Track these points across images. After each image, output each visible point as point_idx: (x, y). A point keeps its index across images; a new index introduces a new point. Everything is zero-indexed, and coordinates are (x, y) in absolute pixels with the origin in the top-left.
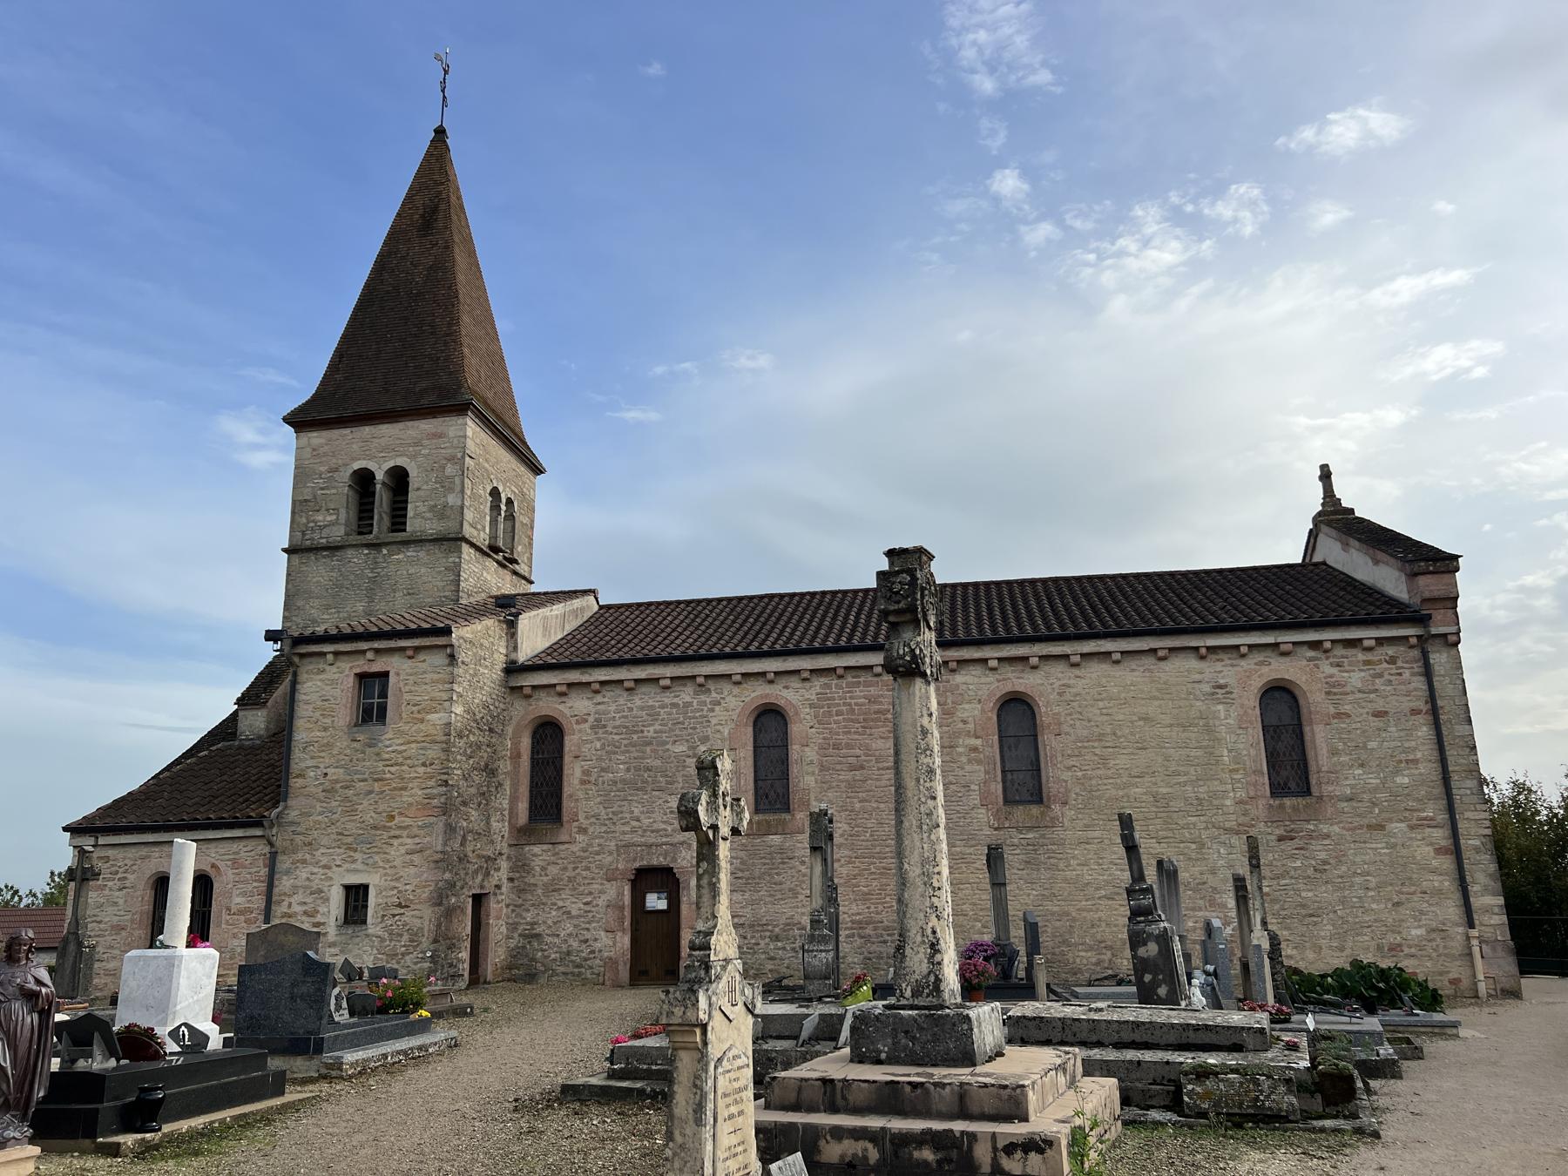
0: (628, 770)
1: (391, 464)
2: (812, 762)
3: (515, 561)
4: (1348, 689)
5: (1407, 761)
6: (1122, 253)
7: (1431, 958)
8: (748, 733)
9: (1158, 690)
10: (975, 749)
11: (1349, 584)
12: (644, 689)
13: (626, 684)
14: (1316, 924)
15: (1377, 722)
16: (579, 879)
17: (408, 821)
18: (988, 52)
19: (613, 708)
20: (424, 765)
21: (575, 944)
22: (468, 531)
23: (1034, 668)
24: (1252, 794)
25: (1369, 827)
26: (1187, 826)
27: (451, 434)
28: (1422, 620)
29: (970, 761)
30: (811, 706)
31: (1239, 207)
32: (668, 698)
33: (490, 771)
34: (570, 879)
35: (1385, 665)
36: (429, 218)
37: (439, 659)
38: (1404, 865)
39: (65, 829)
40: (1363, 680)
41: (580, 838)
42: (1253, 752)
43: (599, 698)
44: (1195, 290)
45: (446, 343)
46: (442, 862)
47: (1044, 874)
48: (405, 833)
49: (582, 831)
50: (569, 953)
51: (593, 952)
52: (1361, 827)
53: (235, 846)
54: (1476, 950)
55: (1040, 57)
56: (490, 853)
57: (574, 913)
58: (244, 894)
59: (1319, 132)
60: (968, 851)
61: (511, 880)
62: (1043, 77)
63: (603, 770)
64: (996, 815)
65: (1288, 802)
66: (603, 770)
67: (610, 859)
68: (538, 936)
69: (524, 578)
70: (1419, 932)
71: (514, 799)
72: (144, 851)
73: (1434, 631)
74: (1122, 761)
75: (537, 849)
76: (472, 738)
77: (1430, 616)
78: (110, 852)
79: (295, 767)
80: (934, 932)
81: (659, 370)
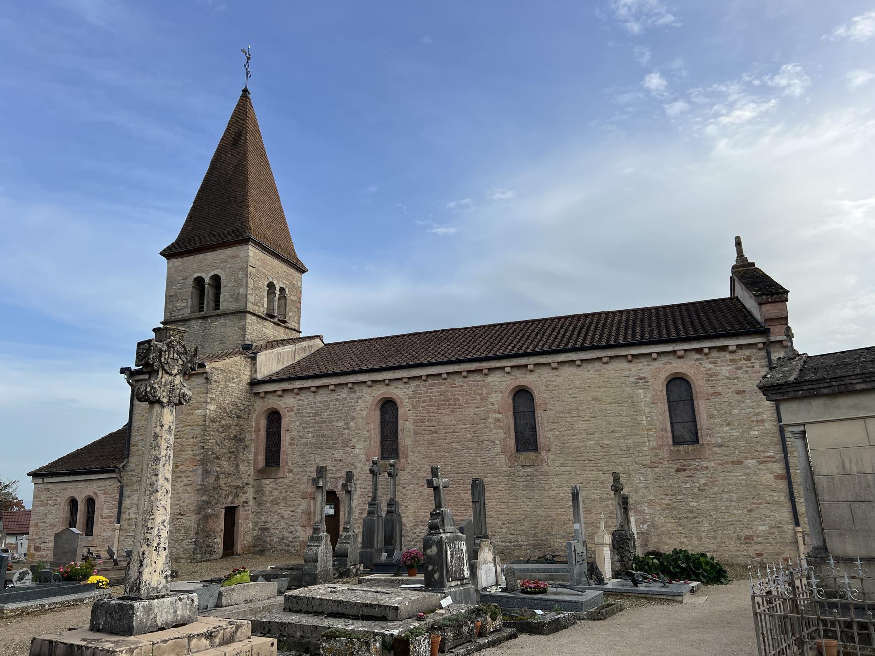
0: (313, 437)
1: (212, 273)
2: (409, 430)
3: (284, 322)
4: (720, 377)
5: (757, 421)
6: (717, 115)
7: (772, 545)
8: (378, 413)
9: (604, 382)
10: (498, 420)
11: (740, 311)
12: (322, 391)
13: (312, 389)
14: (699, 523)
15: (738, 397)
16: (288, 498)
17: (185, 468)
18: (634, 9)
19: (306, 403)
20: (193, 438)
21: (286, 534)
22: (250, 307)
23: (532, 371)
24: (660, 443)
25: (733, 462)
26: (620, 464)
27: (241, 255)
28: (765, 332)
29: (495, 427)
30: (410, 398)
31: (792, 80)
32: (334, 396)
33: (238, 439)
34: (284, 498)
35: (744, 361)
36: (238, 138)
37: (200, 380)
38: (755, 486)
39: (29, 475)
40: (730, 372)
41: (289, 475)
42: (660, 418)
43: (299, 397)
44: (773, 130)
45: (241, 206)
46: (203, 490)
47: (537, 493)
48: (183, 475)
49: (290, 471)
50: (283, 539)
51: (295, 538)
52: (727, 463)
53: (105, 483)
54: (800, 540)
55: (665, 8)
56: (239, 484)
57: (286, 516)
58: (108, 508)
59: (848, 28)
60: (496, 479)
61: (255, 498)
62: (669, 18)
63: (301, 437)
64: (510, 458)
65: (682, 448)
66: (301, 437)
67: (304, 486)
68: (268, 529)
69: (294, 330)
70: (764, 528)
71: (256, 454)
72: (64, 486)
73: (773, 339)
74: (582, 425)
75: (267, 481)
76: (223, 422)
77: (769, 330)
78: (50, 486)
79: (133, 441)
80: (144, 554)
81: (452, 204)
